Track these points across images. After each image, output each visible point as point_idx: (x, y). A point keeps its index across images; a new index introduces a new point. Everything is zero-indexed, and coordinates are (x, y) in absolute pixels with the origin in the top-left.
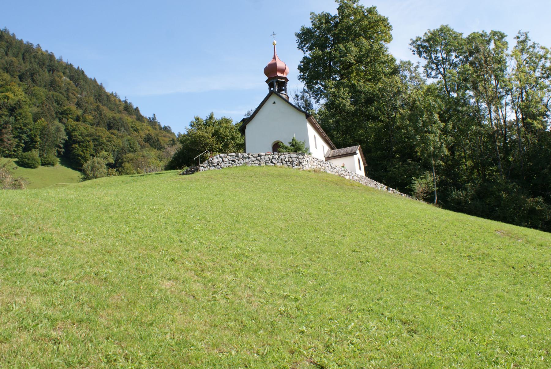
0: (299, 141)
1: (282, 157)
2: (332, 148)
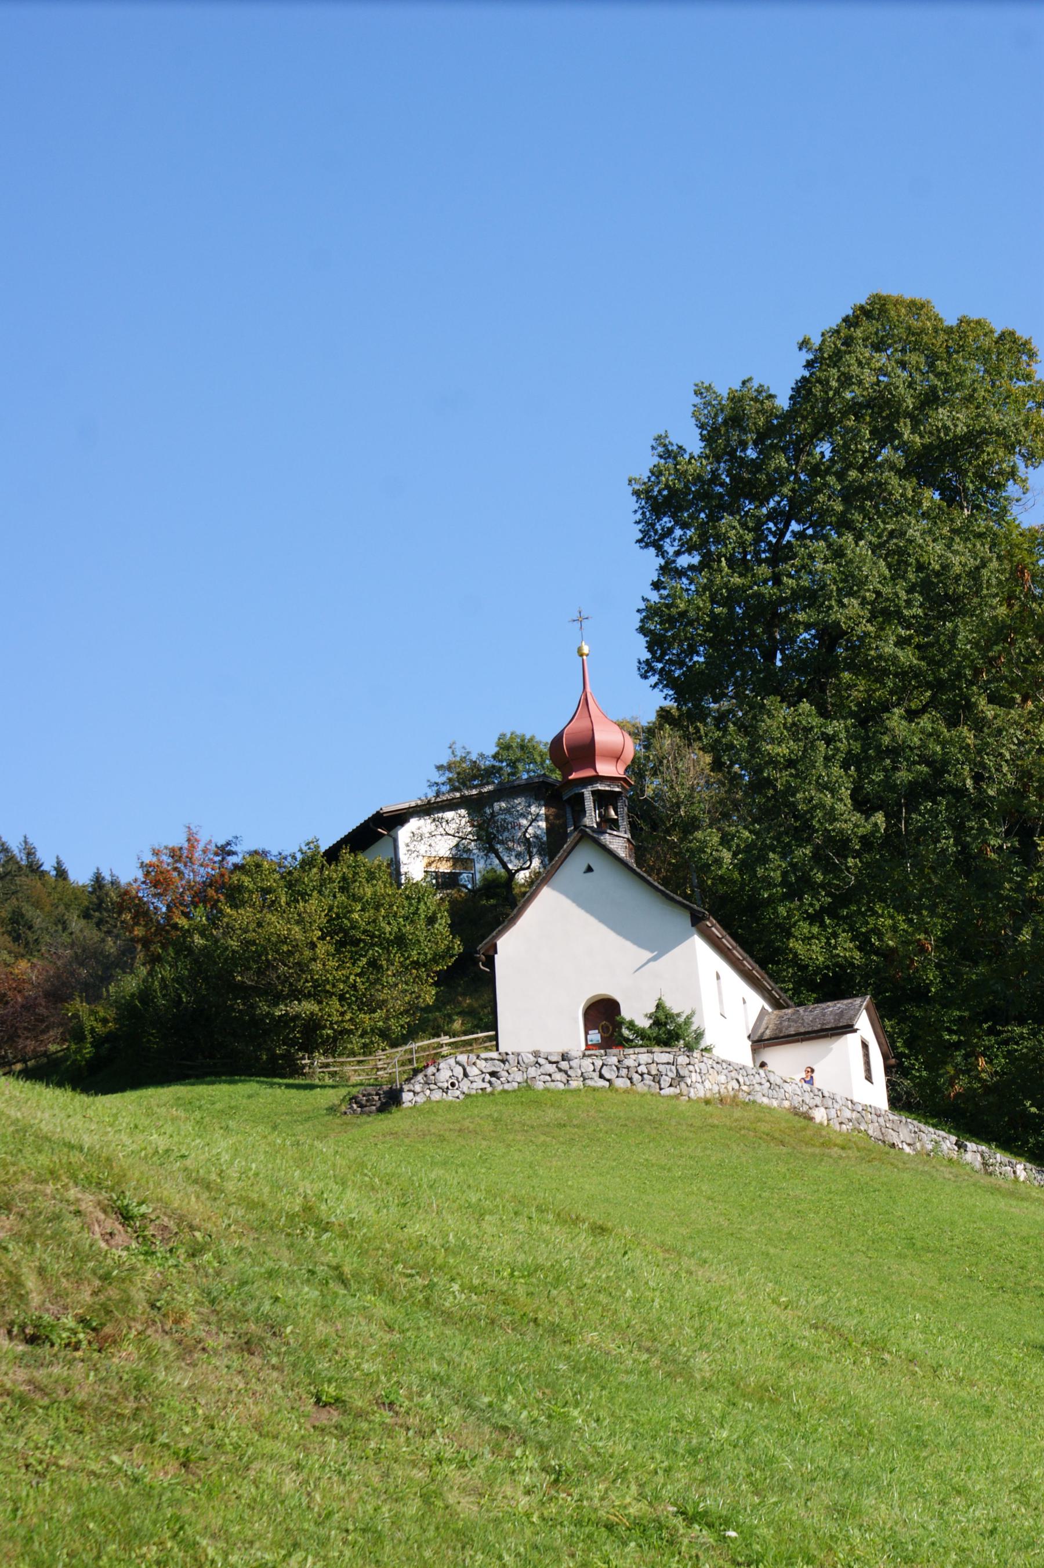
0: (675, 1011)
1: (630, 1062)
2: (777, 1005)
